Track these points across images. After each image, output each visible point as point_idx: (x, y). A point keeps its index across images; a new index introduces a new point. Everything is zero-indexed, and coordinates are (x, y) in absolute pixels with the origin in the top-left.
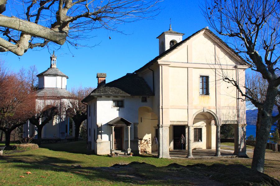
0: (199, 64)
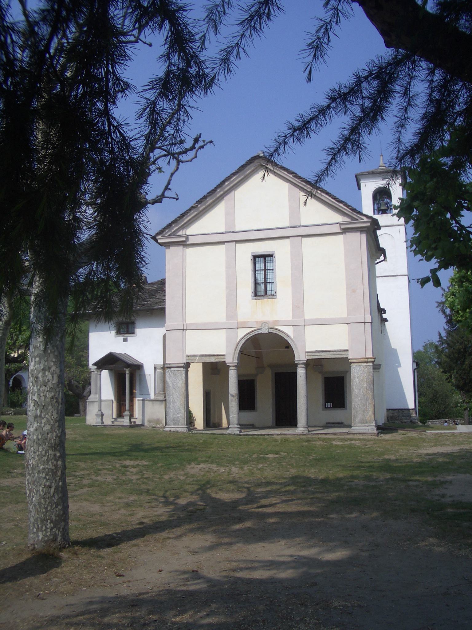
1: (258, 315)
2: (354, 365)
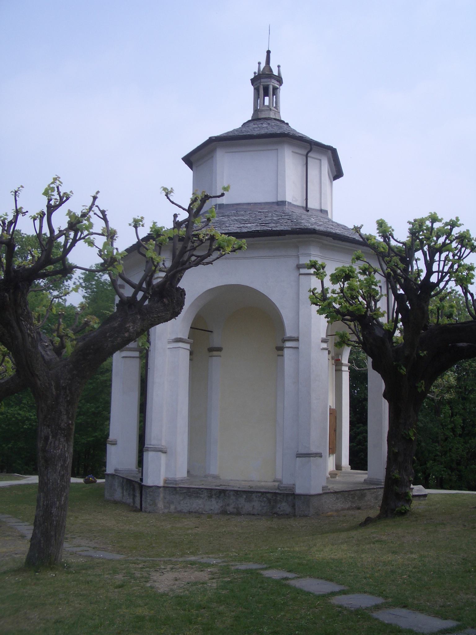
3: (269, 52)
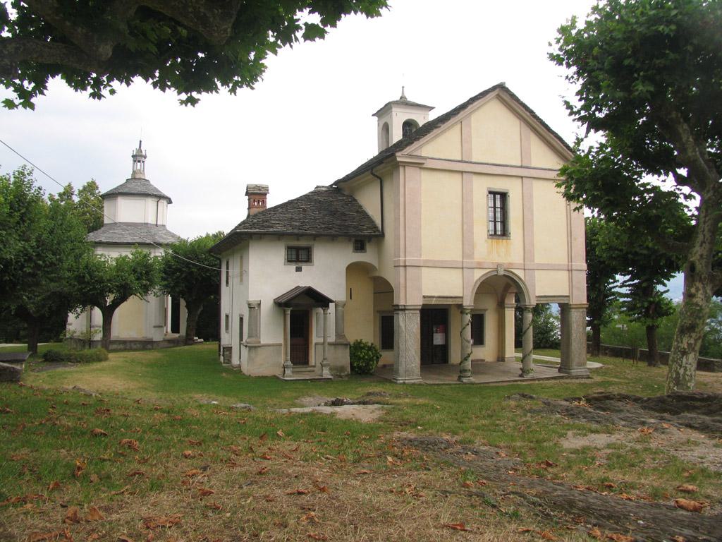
0: (488, 164)
1: (495, 256)
2: (573, 310)
3: (141, 142)
